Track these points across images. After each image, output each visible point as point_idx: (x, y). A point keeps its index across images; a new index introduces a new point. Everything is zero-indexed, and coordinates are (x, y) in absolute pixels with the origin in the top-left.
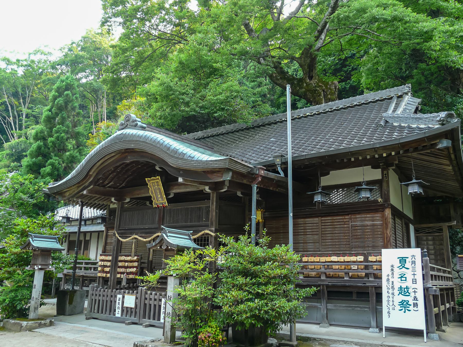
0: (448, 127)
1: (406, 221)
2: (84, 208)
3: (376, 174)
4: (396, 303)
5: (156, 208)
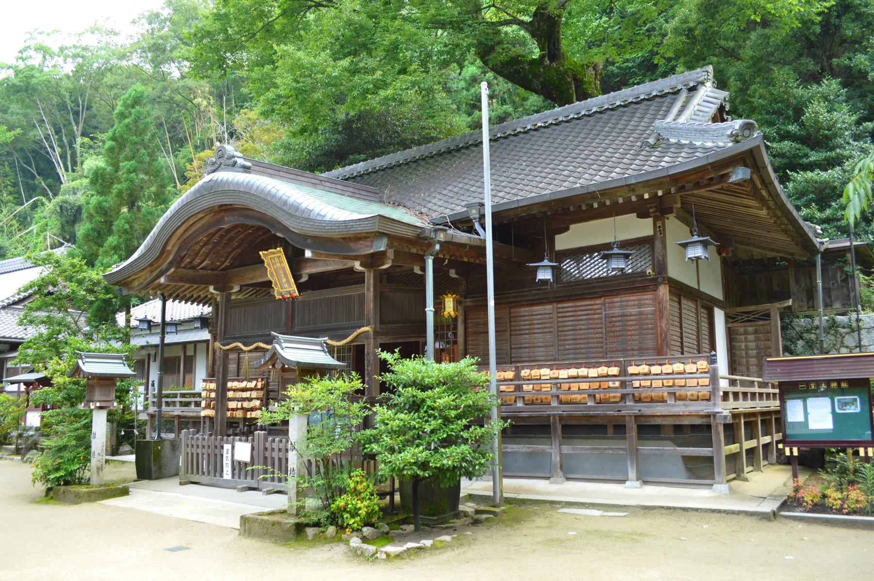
0: (745, 146)
1: (707, 304)
2: (167, 303)
3: (644, 228)
5: (279, 299)
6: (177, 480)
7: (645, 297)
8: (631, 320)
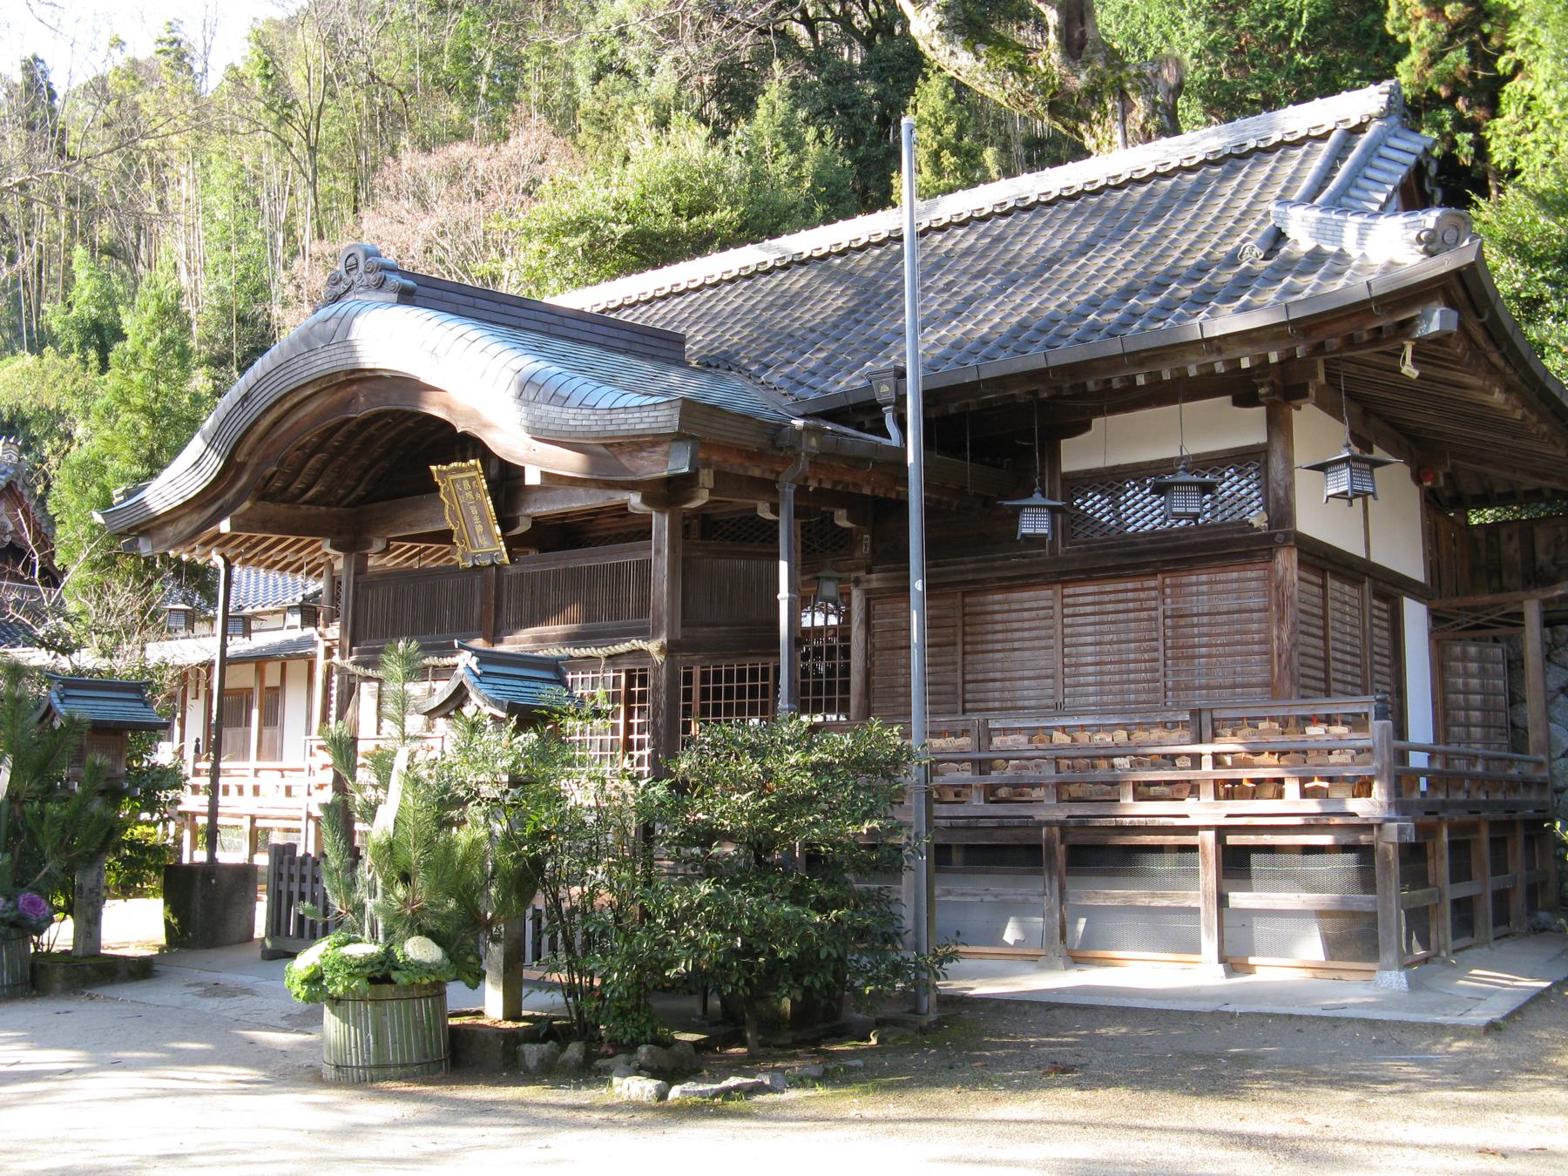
7: (1250, 574)
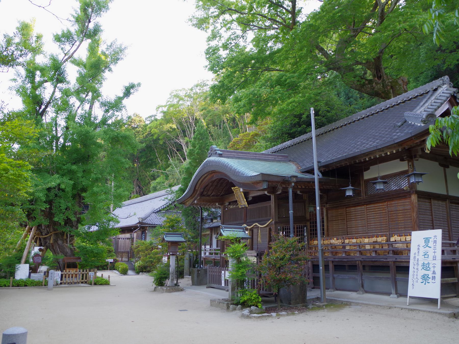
4: (419, 277)
6: (205, 286)
7: (406, 201)
8: (400, 213)
